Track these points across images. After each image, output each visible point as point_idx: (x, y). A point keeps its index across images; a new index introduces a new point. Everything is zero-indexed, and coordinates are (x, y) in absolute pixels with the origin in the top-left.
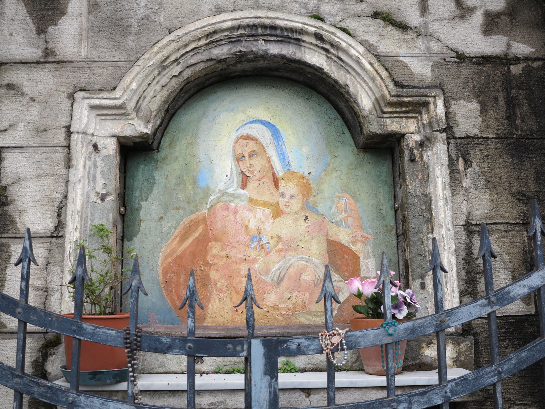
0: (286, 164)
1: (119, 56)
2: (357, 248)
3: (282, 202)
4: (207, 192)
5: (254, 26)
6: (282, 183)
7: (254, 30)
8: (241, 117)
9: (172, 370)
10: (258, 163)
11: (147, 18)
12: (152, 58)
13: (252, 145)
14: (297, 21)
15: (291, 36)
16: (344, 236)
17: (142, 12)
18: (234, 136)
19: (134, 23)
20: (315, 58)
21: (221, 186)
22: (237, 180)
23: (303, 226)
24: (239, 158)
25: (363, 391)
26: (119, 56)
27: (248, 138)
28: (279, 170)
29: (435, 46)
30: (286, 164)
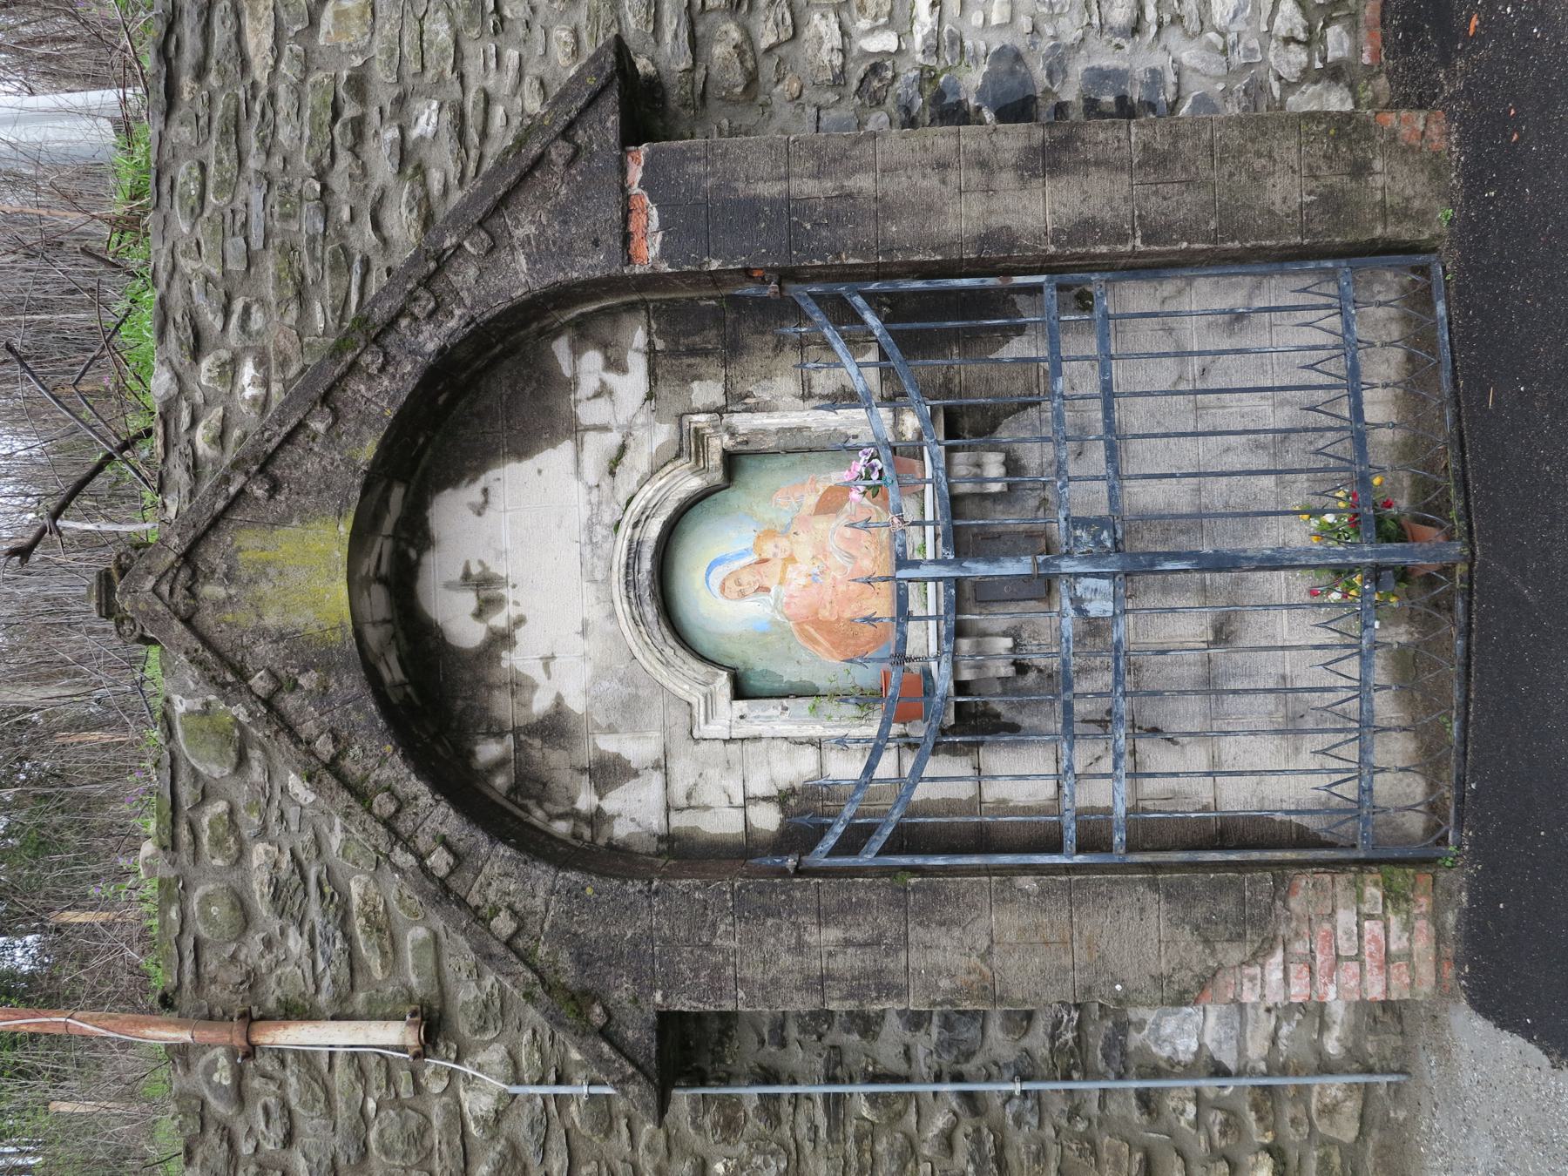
1: (659, 702)
3: (781, 555)
6: (764, 556)
8: (703, 593)
10: (746, 578)
12: (661, 674)
14: (622, 545)
15: (634, 552)
16: (811, 500)
17: (615, 685)
18: (721, 600)
19: (626, 691)
20: (654, 529)
21: (768, 610)
22: (762, 596)
23: (802, 537)
24: (742, 595)
27: (723, 588)
29: (640, 420)
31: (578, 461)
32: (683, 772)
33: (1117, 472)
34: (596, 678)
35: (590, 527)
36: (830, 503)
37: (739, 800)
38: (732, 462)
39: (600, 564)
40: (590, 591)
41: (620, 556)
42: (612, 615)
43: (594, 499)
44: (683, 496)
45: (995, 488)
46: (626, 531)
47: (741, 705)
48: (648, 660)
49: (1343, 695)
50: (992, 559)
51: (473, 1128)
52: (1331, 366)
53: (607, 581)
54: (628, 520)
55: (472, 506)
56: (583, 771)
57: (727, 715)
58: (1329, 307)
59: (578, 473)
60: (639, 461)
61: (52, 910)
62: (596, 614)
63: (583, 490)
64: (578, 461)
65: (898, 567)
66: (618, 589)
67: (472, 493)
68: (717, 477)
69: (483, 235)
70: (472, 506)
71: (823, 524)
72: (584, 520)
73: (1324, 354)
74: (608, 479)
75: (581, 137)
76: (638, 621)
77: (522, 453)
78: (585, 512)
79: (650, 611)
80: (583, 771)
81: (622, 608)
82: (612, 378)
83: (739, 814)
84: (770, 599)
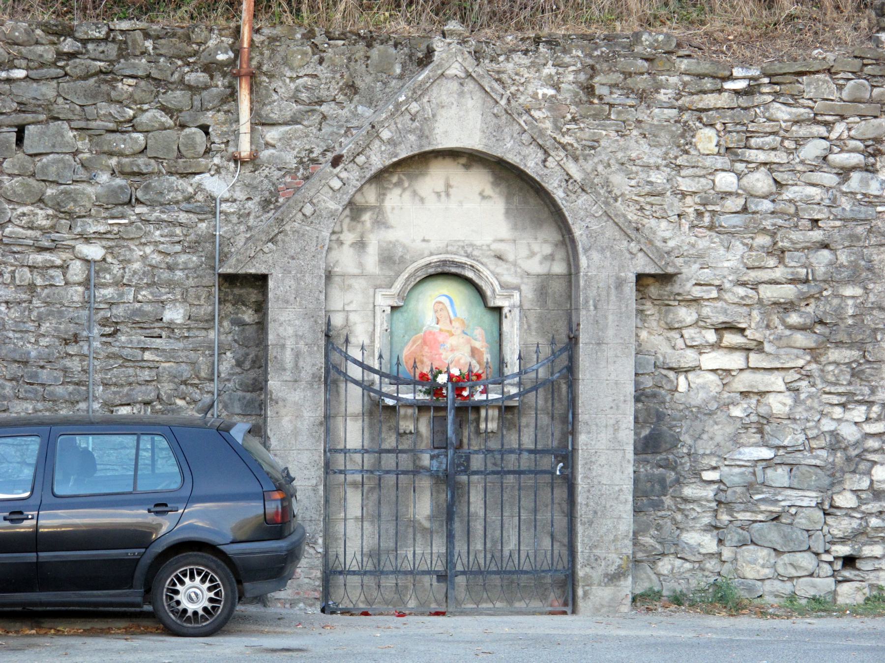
0: (455, 315)
1: (392, 273)
2: (483, 350)
3: (453, 330)
4: (423, 326)
5: (446, 261)
6: (454, 323)
7: (444, 262)
8: (437, 293)
9: (796, 486)
10: (444, 313)
11: (402, 256)
12: (405, 275)
13: (441, 305)
14: (463, 260)
15: (461, 265)
16: (478, 344)
17: (400, 254)
18: (434, 302)
19: (397, 258)
20: (470, 274)
21: (428, 323)
22: (435, 321)
23: (461, 340)
24: (436, 312)
25: (487, 526)
26: (392, 273)
27: (440, 303)
28: (452, 317)
29: (519, 270)
30: (455, 315)
31: (502, 241)
32: (359, 284)
33: (488, 474)
34: (404, 246)
35: (472, 245)
36: (474, 352)
37: (347, 308)
38: (498, 310)
39: (454, 249)
40: (442, 245)
41: (458, 259)
42: (431, 254)
43: (484, 247)
44: (484, 288)
45: (483, 426)
46: (469, 261)
47: (389, 310)
48: (411, 269)
49: (394, 564)
50: (454, 422)
51: (198, 177)
52: (511, 564)
53: (447, 253)
54: (474, 263)
55: (483, 191)
56: (362, 237)
57: (384, 301)
58: (552, 564)
59: (495, 241)
60: (502, 268)
61: (332, 340)
62: (433, 246)
63: (488, 242)
64: (502, 241)
65: (703, 213)
66: (443, 257)
67: (489, 191)
68: (491, 304)
69: (600, 213)
70: (483, 191)
71: (467, 350)
72: (475, 243)
73: (516, 562)
74: (493, 254)
75: (640, 255)
76: (428, 265)
77: (508, 212)
78: (478, 243)
79: (431, 271)
80: (362, 237)
81: (435, 258)
82: (538, 258)
83: (340, 307)
84: (434, 324)
